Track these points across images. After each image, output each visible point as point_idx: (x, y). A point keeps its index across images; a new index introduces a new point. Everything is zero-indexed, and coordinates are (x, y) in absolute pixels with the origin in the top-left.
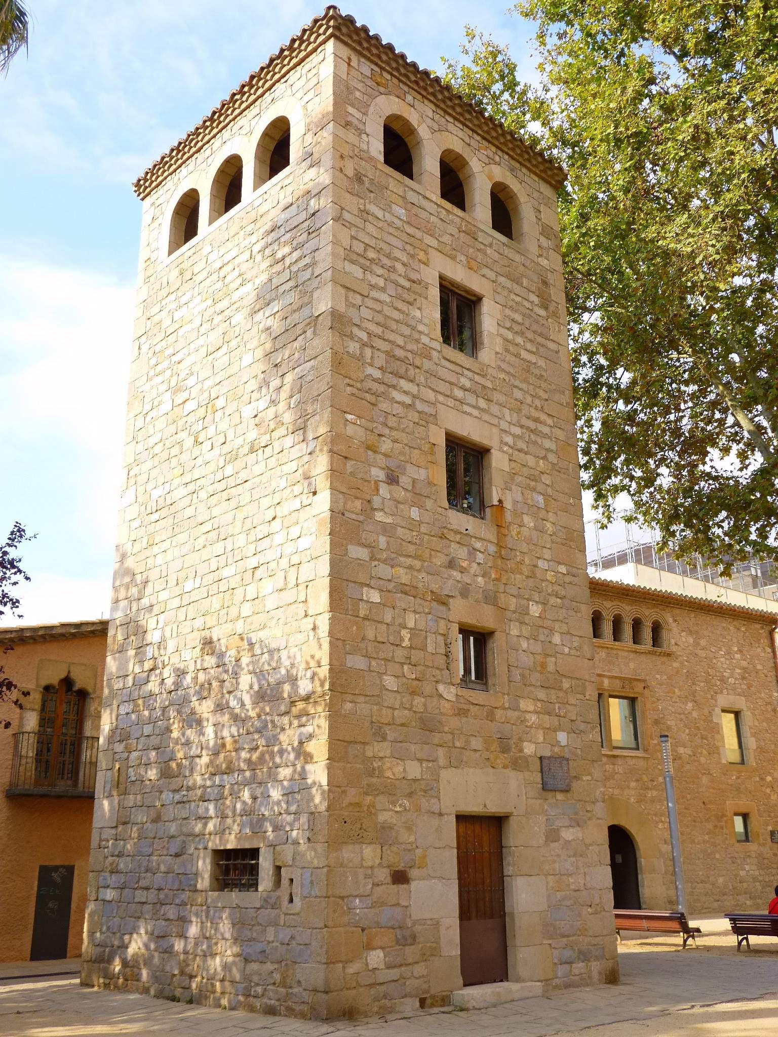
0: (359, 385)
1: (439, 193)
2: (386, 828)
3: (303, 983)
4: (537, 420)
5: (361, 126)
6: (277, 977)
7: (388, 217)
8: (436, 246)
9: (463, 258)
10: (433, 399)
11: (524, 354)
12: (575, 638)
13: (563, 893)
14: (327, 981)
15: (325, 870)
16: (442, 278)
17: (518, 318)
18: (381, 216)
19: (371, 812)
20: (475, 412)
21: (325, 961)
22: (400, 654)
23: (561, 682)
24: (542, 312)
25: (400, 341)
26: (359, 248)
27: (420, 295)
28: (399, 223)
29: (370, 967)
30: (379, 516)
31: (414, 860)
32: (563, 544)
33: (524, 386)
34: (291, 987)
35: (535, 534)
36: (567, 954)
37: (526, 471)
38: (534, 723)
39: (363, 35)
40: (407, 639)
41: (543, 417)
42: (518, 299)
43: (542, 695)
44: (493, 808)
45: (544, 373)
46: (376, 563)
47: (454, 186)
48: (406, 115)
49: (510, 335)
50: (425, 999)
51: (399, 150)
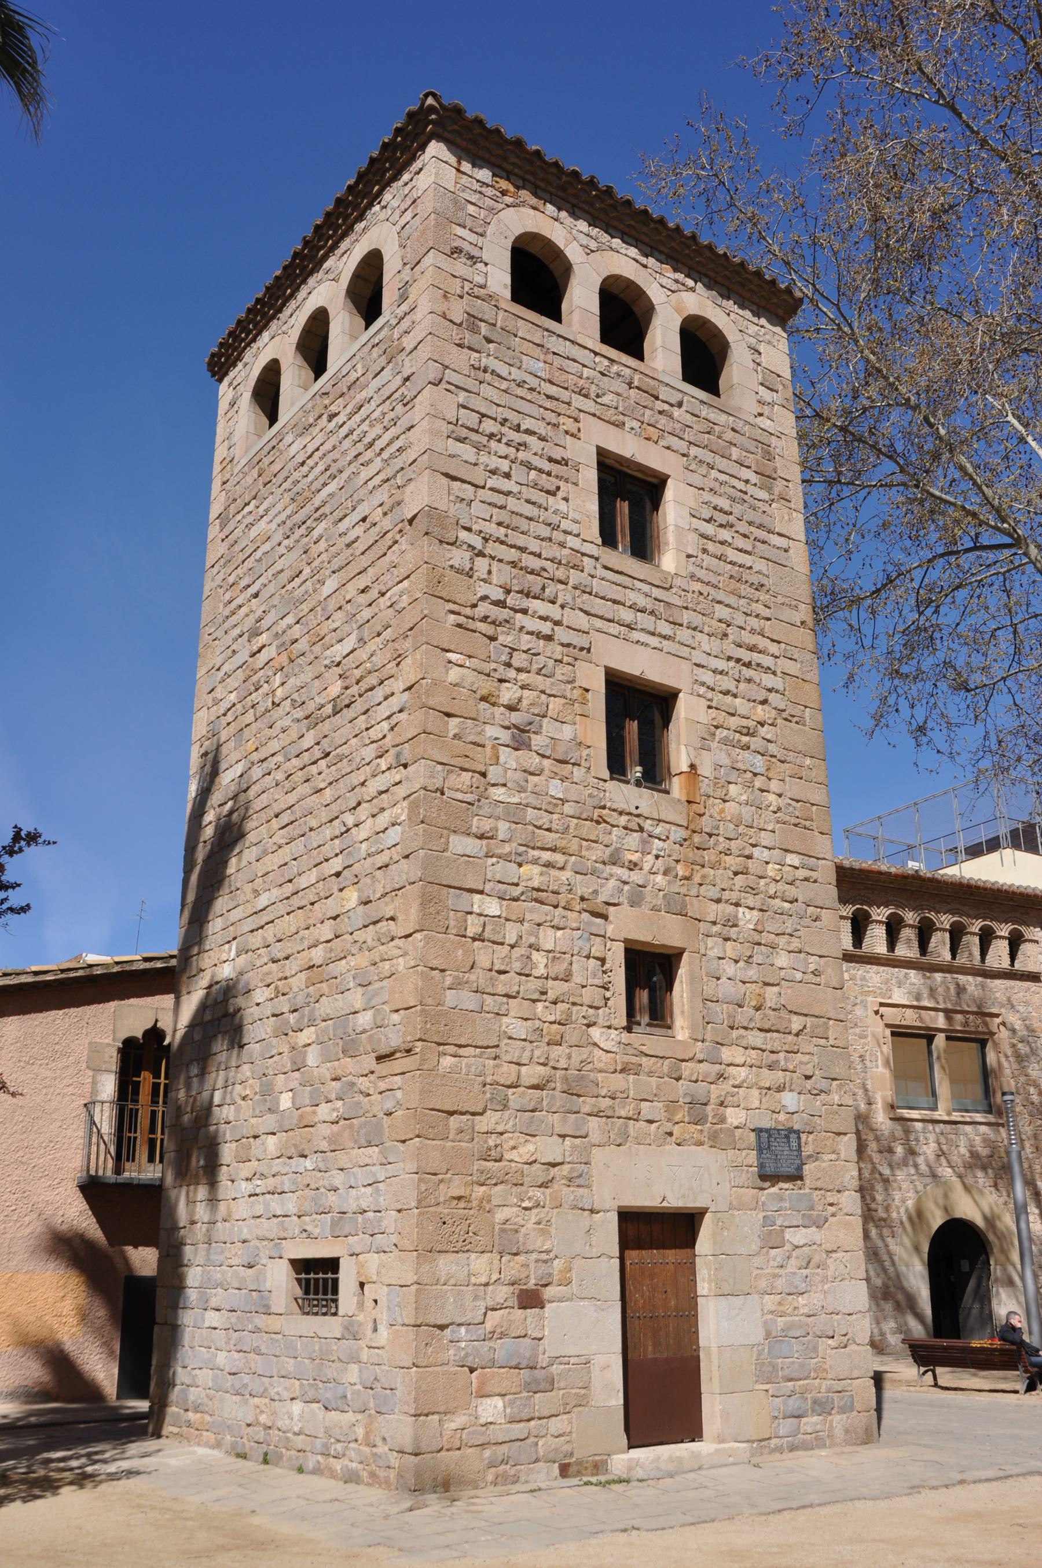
0: (468, 611)
1: (598, 336)
2: (509, 1230)
3: (388, 1439)
4: (752, 649)
5: (475, 252)
6: (360, 1432)
7: (516, 374)
8: (592, 411)
9: (636, 424)
10: (585, 627)
11: (732, 555)
12: (812, 959)
13: (788, 1319)
14: (416, 1438)
15: (414, 1287)
16: (601, 452)
17: (724, 503)
18: (504, 374)
19: (485, 1207)
20: (654, 641)
21: (412, 1412)
22: (531, 986)
23: (790, 1021)
24: (763, 495)
25: (534, 546)
26: (472, 420)
27: (567, 481)
28: (533, 382)
29: (483, 1421)
30: (498, 793)
31: (550, 1275)
32: (795, 825)
33: (732, 600)
34: (375, 1446)
35: (747, 812)
36: (793, 1404)
37: (734, 722)
38: (744, 1081)
39: (478, 130)
40: (542, 966)
41: (763, 643)
42: (723, 477)
43: (756, 1038)
44: (675, 1201)
45: (764, 581)
46: (494, 860)
47: (624, 319)
48: (546, 233)
49: (709, 529)
50: (569, 1465)
51: (538, 279)
